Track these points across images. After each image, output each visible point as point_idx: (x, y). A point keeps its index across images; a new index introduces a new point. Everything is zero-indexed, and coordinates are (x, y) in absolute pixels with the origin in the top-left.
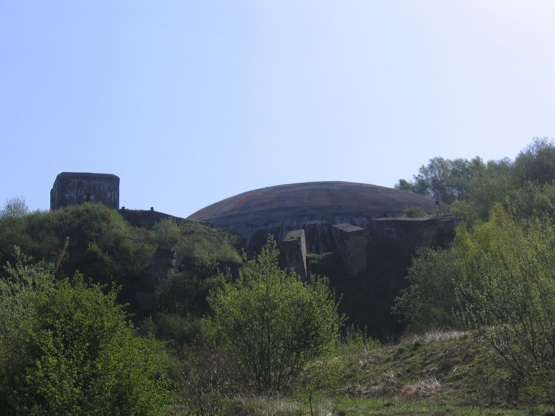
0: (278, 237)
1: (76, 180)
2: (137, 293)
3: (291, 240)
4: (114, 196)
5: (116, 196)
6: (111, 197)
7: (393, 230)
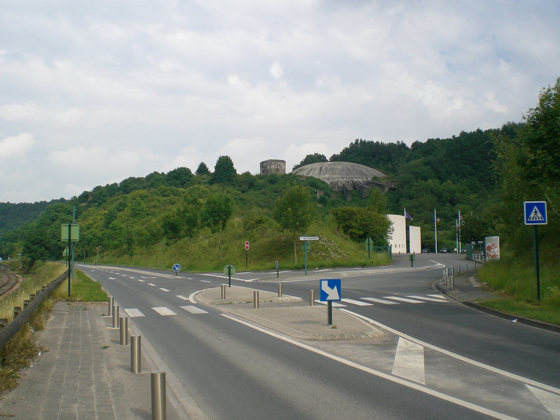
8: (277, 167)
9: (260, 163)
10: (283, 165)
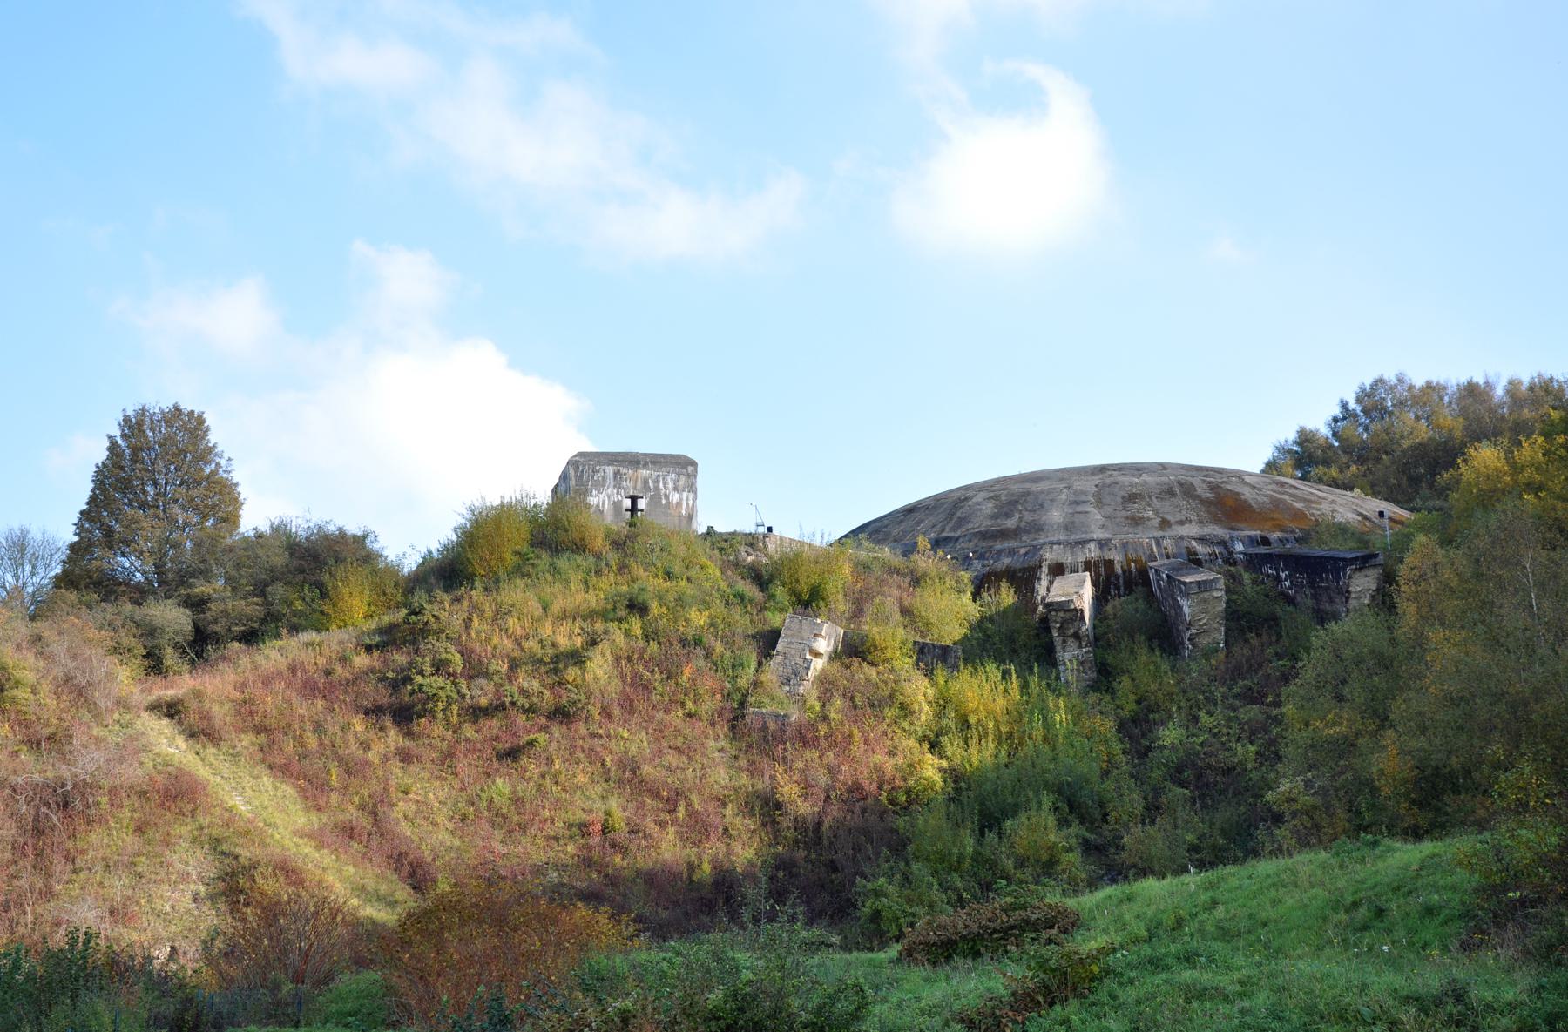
3: (1063, 599)
4: (687, 499)
5: (691, 502)
6: (679, 504)
7: (1283, 575)
8: (634, 499)
10: (676, 489)
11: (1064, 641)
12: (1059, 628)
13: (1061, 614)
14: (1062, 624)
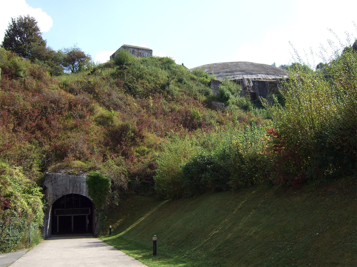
0: (244, 84)
1: (132, 49)
2: (212, 102)
9: (111, 57)
11: (270, 92)
12: (270, 89)
13: (272, 85)
14: (271, 87)
